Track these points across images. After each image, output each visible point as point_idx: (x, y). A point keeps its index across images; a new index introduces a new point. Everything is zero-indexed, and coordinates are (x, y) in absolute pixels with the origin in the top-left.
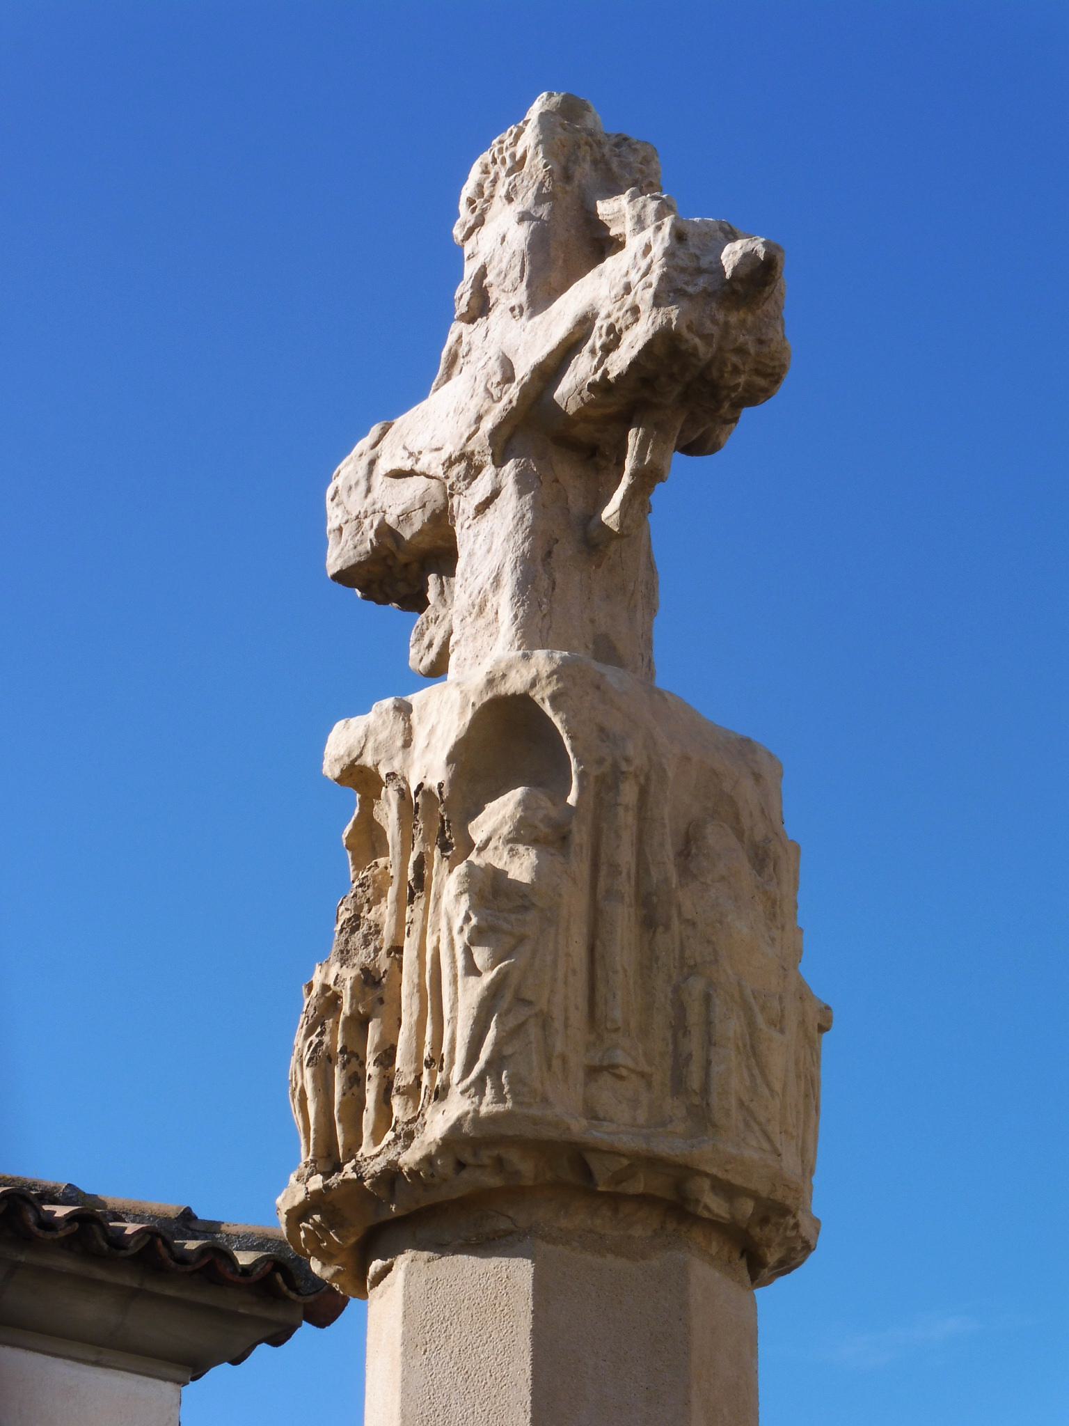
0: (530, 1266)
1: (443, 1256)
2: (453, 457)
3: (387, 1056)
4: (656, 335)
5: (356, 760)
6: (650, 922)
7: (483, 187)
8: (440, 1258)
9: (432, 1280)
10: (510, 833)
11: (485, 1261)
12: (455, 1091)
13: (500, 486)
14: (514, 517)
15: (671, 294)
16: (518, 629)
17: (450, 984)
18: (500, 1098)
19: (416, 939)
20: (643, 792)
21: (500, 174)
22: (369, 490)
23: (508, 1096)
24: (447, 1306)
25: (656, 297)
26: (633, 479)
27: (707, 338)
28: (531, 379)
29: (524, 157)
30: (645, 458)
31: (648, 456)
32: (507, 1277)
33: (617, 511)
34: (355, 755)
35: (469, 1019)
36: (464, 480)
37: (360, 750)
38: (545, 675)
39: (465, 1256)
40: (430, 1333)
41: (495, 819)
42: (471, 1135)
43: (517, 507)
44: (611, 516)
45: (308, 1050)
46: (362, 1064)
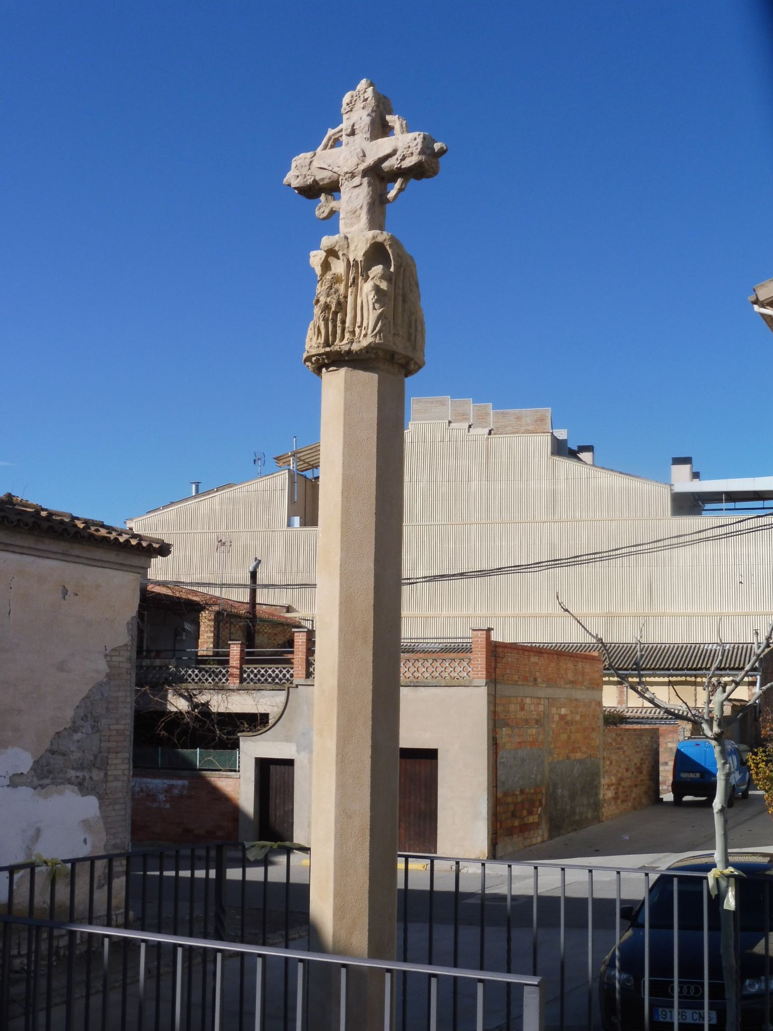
3: (343, 322)
6: (404, 301)
12: (369, 335)
18: (380, 339)
20: (404, 270)
22: (309, 169)
25: (419, 152)
27: (428, 164)
29: (367, 99)
46: (336, 322)
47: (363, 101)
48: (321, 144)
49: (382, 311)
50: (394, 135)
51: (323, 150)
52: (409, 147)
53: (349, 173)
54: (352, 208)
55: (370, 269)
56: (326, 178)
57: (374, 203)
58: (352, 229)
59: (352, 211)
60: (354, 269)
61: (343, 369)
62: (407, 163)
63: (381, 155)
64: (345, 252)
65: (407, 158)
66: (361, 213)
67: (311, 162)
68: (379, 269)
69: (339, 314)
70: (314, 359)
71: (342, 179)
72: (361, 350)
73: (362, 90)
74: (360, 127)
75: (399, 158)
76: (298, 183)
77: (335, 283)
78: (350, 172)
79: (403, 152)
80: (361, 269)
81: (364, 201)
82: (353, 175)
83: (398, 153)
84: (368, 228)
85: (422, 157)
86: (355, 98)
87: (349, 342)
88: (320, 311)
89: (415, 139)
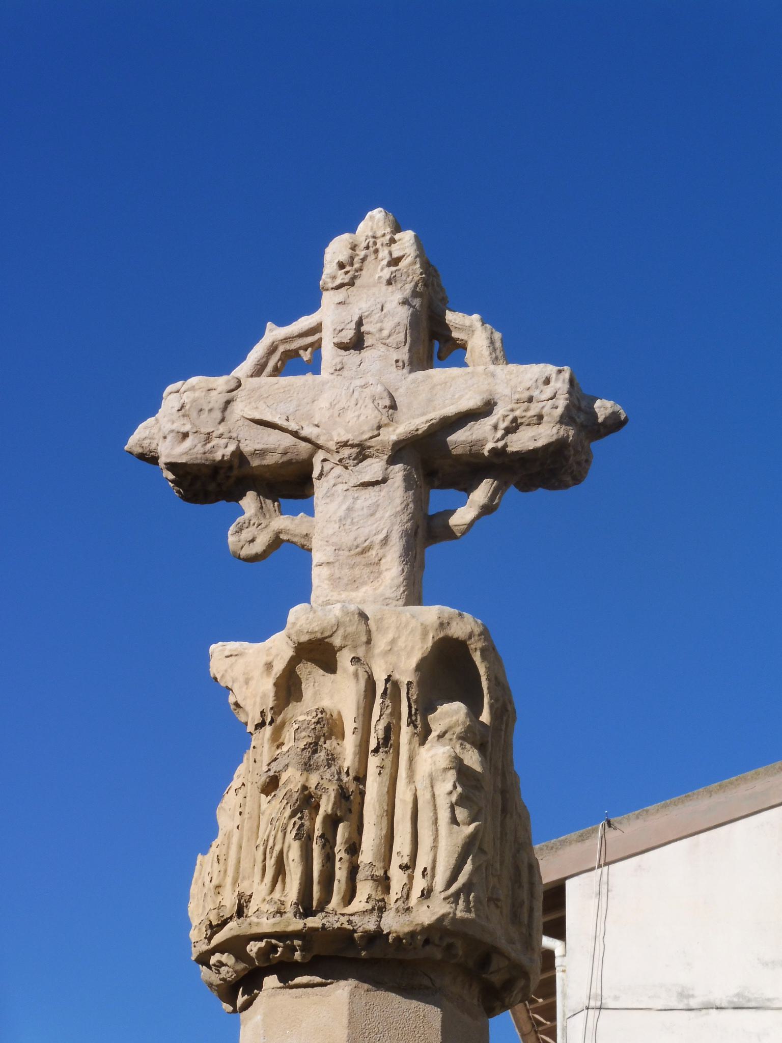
0: (439, 1013)
1: (378, 990)
2: (349, 443)
3: (354, 849)
4: (557, 441)
5: (326, 638)
7: (354, 260)
8: (376, 991)
9: (370, 1004)
10: (461, 733)
11: (408, 1001)
13: (388, 477)
14: (402, 503)
15: (567, 418)
16: (404, 580)
17: (433, 824)
18: (468, 909)
19: (387, 780)
21: (369, 257)
23: (473, 910)
24: (381, 1024)
25: (562, 417)
26: (482, 509)
28: (437, 423)
30: (495, 501)
31: (496, 500)
32: (424, 1016)
33: (466, 524)
34: (327, 634)
35: (455, 853)
36: (354, 459)
37: (331, 633)
38: (477, 633)
39: (394, 994)
40: (368, 1039)
41: (450, 719)
42: (448, 927)
43: (404, 497)
44: (459, 525)
45: (294, 827)
47: (389, 264)
48: (244, 358)
49: (477, 830)
50: (465, 365)
51: (252, 376)
52: (530, 400)
53: (353, 446)
54: (355, 539)
55: (434, 710)
56: (274, 451)
57: (416, 533)
58: (354, 594)
59: (357, 547)
60: (388, 702)
61: (342, 983)
62: (523, 441)
63: (451, 410)
64: (361, 652)
65: (521, 428)
66: (384, 556)
67: (228, 403)
68: (457, 712)
69: (341, 826)
70: (253, 948)
71: (324, 460)
72: (412, 934)
73: (384, 235)
74: (381, 330)
75: (502, 425)
76: (186, 453)
77: (327, 737)
78: (356, 442)
79: (512, 410)
80: (410, 707)
81: (393, 525)
82: (362, 452)
83: (499, 411)
84: (404, 596)
85: (567, 431)
86: (362, 254)
87: (373, 909)
88: (288, 812)
89: (547, 381)
